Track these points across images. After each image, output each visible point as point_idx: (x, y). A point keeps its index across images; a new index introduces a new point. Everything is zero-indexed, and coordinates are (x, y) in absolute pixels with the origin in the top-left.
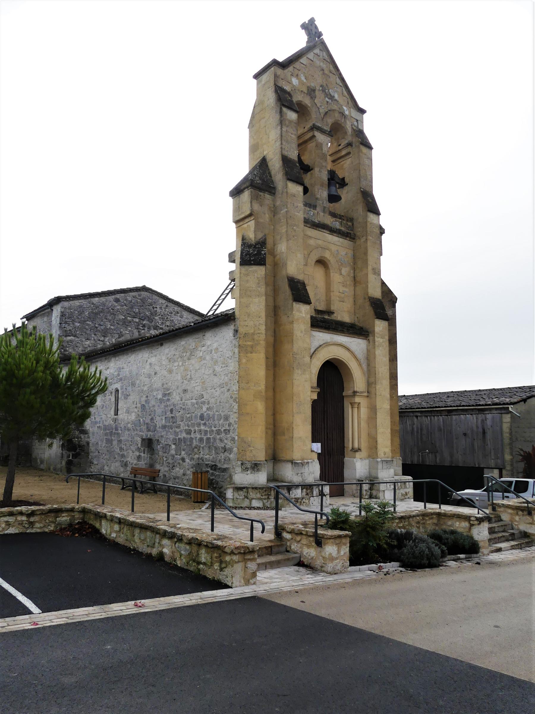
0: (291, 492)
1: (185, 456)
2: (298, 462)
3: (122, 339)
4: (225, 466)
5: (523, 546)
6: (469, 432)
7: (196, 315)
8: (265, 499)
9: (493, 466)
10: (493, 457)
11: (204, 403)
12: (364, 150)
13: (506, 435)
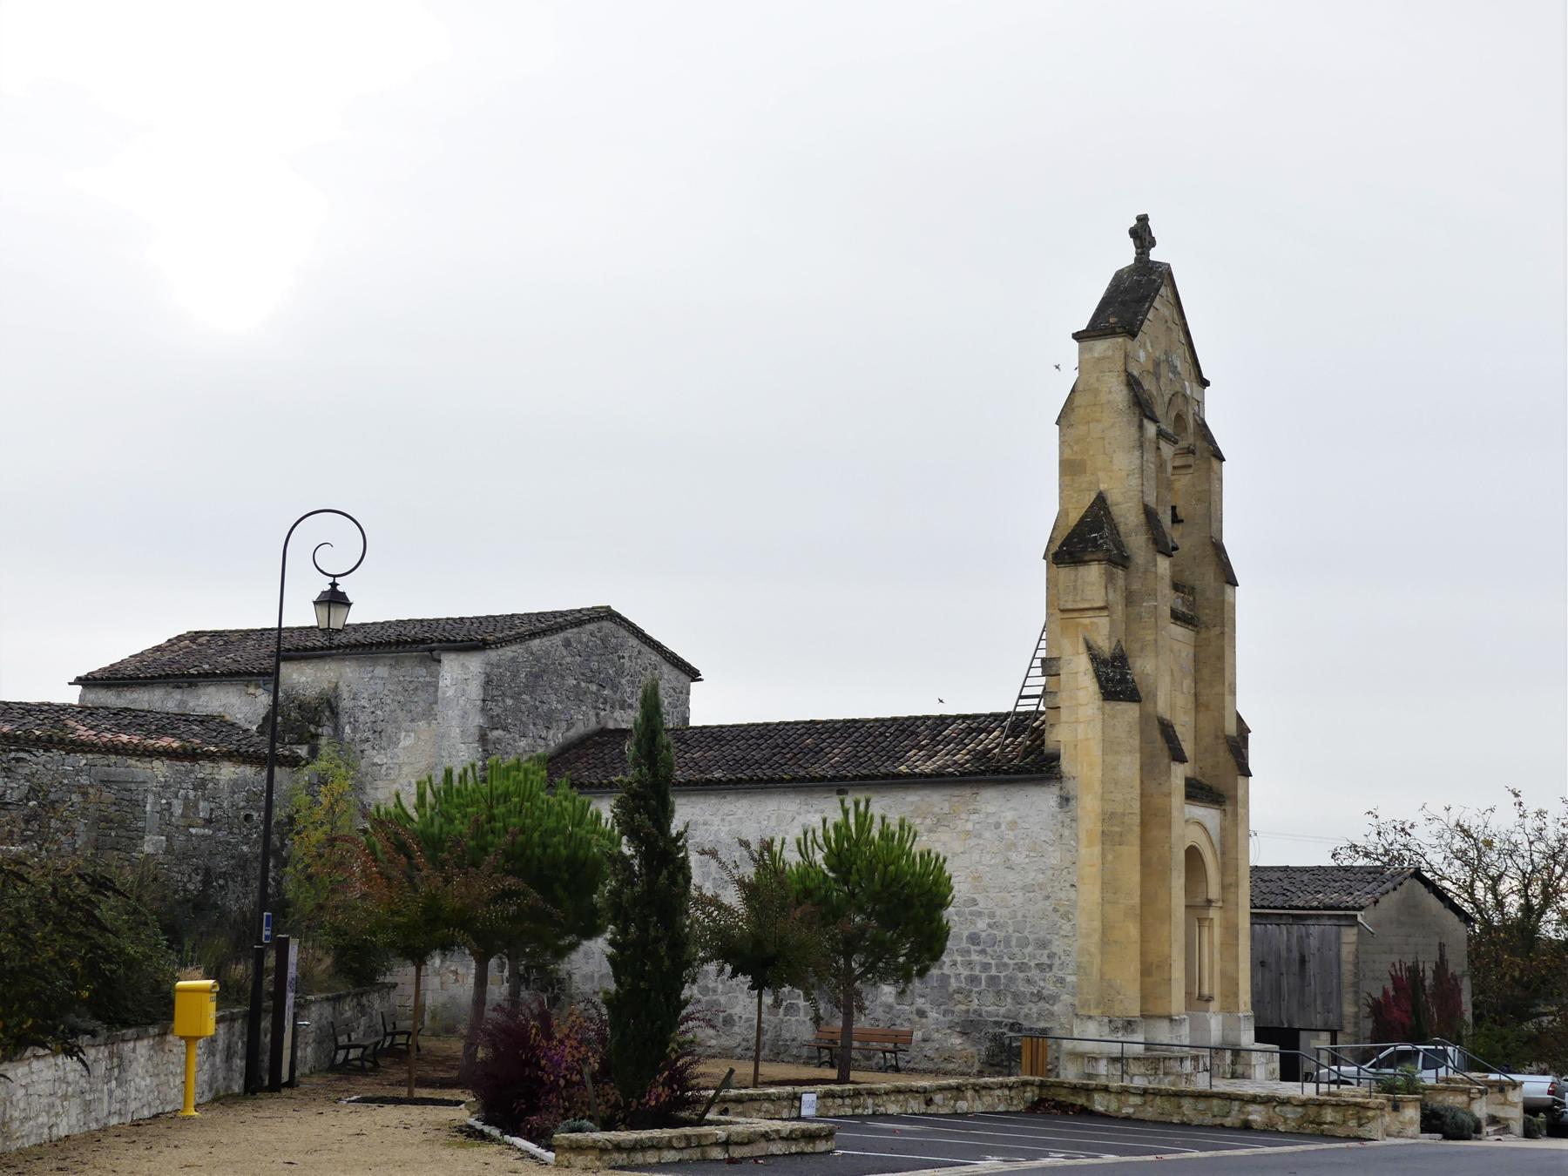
1: (927, 1007)
3: (572, 733)
4: (1042, 1025)
6: (1271, 960)
9: (1319, 1025)
10: (1319, 1009)
11: (980, 914)
12: (1215, 462)
13: (1347, 968)
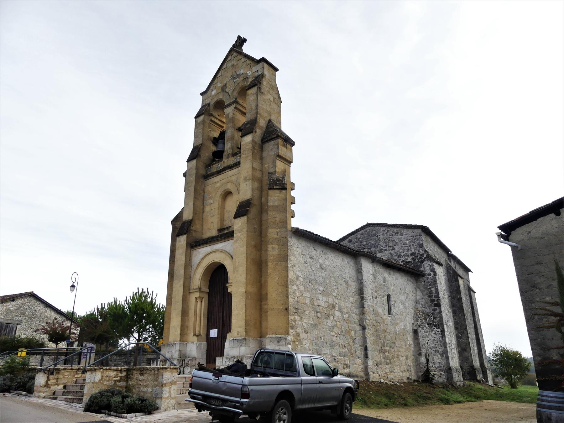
5: (75, 401)
7: (414, 228)
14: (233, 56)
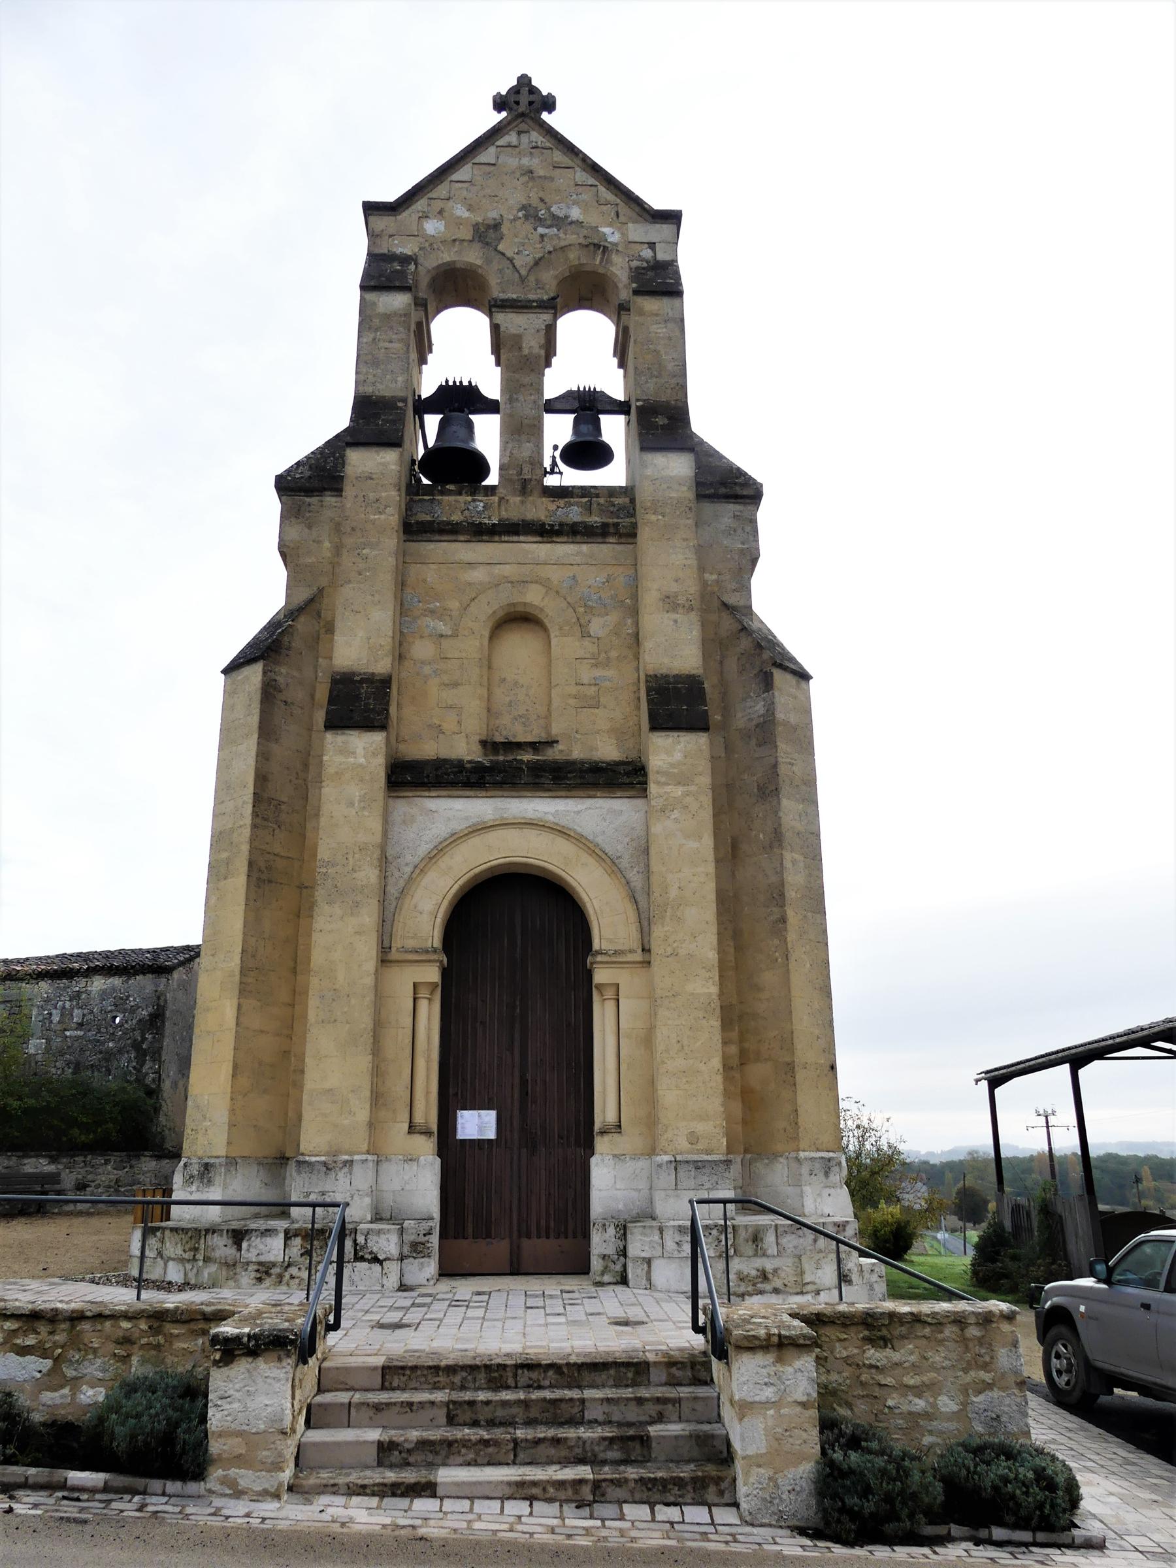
0: (244, 1245)
2: (313, 1159)
8: (189, 1261)
14: (525, 139)
